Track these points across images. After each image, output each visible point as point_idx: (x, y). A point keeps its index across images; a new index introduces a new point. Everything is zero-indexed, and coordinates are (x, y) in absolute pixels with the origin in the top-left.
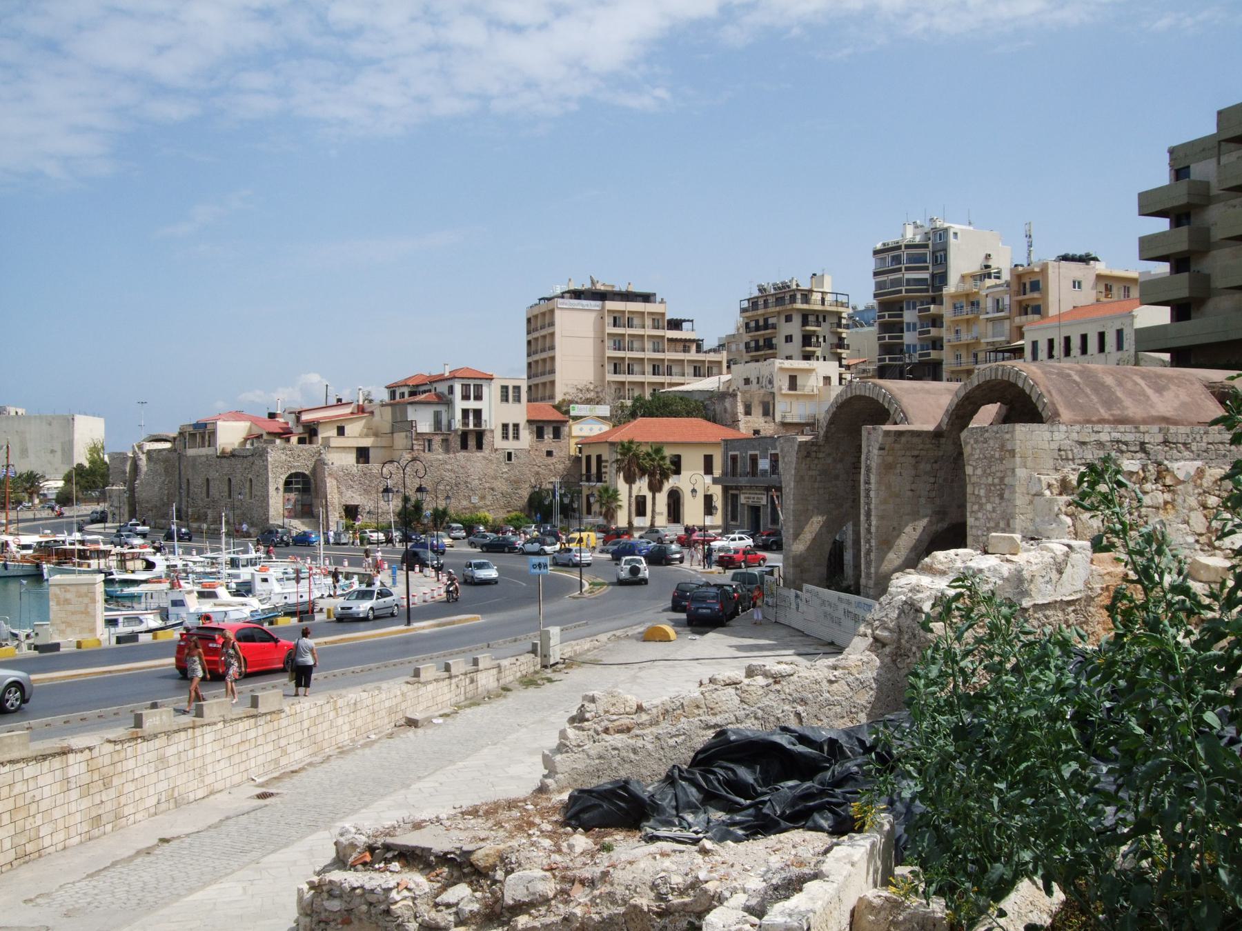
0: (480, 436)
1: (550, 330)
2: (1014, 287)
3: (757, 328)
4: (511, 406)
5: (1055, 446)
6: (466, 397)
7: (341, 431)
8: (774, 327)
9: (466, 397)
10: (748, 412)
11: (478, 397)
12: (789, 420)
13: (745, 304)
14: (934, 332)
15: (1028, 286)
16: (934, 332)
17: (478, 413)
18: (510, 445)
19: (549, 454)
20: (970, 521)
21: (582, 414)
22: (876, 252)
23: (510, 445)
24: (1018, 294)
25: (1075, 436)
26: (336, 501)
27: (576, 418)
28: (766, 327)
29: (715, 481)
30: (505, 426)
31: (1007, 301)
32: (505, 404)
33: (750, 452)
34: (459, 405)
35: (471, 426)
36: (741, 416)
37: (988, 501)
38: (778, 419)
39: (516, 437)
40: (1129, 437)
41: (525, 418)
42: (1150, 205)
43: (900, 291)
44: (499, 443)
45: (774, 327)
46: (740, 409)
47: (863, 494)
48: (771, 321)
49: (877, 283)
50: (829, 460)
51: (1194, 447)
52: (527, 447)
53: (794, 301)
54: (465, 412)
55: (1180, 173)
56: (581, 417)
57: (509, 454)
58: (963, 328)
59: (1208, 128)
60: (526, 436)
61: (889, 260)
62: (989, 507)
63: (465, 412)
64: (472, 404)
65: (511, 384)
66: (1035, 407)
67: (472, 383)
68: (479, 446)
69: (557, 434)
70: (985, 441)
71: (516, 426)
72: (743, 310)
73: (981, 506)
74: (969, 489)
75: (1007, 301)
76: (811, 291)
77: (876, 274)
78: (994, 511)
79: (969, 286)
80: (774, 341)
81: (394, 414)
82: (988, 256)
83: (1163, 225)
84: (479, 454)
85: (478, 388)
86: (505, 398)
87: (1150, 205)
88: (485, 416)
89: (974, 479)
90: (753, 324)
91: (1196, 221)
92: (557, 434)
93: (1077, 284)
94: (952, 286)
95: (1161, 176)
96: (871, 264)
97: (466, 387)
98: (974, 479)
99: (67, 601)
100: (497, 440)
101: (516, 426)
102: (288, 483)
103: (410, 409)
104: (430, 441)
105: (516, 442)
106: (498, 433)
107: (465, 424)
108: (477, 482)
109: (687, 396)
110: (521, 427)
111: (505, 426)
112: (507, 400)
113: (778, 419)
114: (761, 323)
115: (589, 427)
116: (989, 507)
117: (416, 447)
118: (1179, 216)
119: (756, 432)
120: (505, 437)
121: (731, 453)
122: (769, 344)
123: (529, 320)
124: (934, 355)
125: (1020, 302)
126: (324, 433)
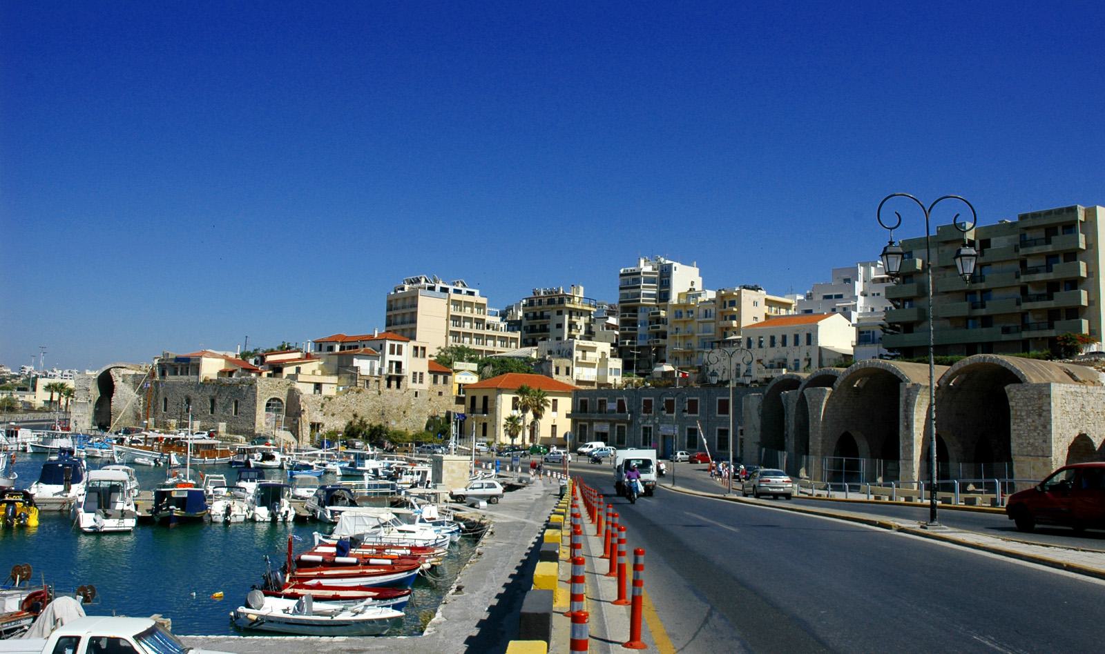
0: (399, 379)
1: (413, 310)
2: (719, 302)
3: (535, 317)
4: (419, 359)
6: (392, 352)
8: (549, 317)
9: (392, 352)
10: (557, 373)
11: (399, 353)
12: (581, 379)
15: (727, 303)
17: (399, 364)
18: (417, 386)
19: (440, 394)
20: (1013, 427)
21: (461, 368)
23: (417, 386)
24: (720, 307)
26: (307, 419)
27: (457, 371)
28: (542, 317)
30: (415, 373)
31: (713, 311)
32: (416, 358)
33: (598, 399)
34: (388, 357)
35: (394, 373)
37: (1028, 416)
38: (575, 378)
39: (421, 382)
41: (427, 370)
43: (639, 301)
44: (411, 385)
45: (549, 317)
46: (554, 370)
48: (545, 314)
49: (621, 294)
50: (836, 401)
52: (427, 389)
54: (391, 362)
56: (1068, 374)
57: (416, 393)
58: (681, 326)
60: (428, 378)
61: (630, 281)
63: (391, 362)
64: (396, 358)
65: (509, 348)
66: (1017, 377)
67: (396, 343)
68: (398, 386)
69: (445, 381)
74: (1012, 412)
75: (713, 311)
79: (683, 301)
80: (548, 327)
81: (339, 361)
82: (692, 283)
84: (398, 391)
85: (400, 347)
90: (531, 315)
93: (755, 304)
94: (674, 299)
96: (618, 282)
97: (392, 347)
99: (453, 471)
100: (408, 382)
102: (268, 405)
104: (368, 381)
105: (421, 385)
107: (390, 370)
108: (395, 410)
109: (505, 359)
110: (424, 375)
111: (415, 373)
112: (417, 356)
113: (575, 378)
114: (538, 314)
115: (465, 377)
116: (1029, 420)
117: (359, 385)
120: (414, 381)
121: (580, 399)
122: (544, 329)
125: (722, 313)
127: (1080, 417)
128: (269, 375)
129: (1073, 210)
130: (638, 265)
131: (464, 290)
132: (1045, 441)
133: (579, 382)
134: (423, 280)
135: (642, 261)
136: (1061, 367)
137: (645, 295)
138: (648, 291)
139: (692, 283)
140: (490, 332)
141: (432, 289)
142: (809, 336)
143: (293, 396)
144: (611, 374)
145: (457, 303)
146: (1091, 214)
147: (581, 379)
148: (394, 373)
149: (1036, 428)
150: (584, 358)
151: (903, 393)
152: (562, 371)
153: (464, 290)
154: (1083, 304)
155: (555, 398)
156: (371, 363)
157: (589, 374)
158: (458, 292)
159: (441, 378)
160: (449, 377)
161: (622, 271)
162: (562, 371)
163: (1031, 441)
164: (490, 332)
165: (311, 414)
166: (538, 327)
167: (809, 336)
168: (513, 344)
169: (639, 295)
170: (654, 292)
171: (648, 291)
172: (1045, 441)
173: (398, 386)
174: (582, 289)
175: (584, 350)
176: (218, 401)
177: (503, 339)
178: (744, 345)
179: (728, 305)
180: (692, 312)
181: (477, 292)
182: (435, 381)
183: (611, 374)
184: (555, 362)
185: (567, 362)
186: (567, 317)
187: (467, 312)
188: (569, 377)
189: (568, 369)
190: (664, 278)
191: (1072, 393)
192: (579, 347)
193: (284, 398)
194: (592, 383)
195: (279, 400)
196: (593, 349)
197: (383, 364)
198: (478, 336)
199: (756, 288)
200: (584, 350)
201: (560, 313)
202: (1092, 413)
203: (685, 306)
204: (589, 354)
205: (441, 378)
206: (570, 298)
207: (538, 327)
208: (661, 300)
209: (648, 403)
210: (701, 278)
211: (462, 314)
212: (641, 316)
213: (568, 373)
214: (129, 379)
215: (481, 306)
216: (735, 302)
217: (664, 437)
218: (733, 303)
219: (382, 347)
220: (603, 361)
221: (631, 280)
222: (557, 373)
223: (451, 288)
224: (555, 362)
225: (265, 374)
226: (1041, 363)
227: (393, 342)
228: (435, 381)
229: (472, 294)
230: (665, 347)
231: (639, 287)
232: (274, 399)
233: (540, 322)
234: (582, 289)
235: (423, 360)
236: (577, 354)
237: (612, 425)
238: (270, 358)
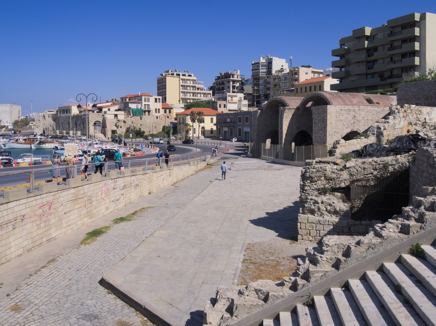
1: (165, 84)
3: (220, 84)
5: (336, 110)
6: (145, 101)
7: (109, 110)
9: (145, 101)
10: (220, 107)
13: (216, 78)
14: (268, 86)
16: (268, 86)
18: (158, 114)
20: (314, 128)
22: (253, 64)
23: (158, 114)
25: (340, 108)
29: (215, 125)
30: (156, 109)
34: (144, 103)
36: (218, 108)
37: (319, 123)
38: (228, 109)
39: (159, 112)
40: (351, 108)
42: (335, 53)
46: (218, 106)
47: (279, 123)
51: (365, 111)
53: (230, 77)
55: (342, 45)
59: (351, 34)
62: (319, 125)
64: (147, 103)
67: (147, 97)
68: (149, 115)
69: (170, 112)
70: (318, 109)
71: (159, 109)
72: (216, 79)
73: (317, 125)
74: (314, 121)
75: (288, 78)
76: (234, 75)
77: (252, 70)
78: (321, 125)
82: (282, 66)
83: (338, 58)
84: (149, 116)
85: (148, 99)
86: (156, 101)
87: (335, 53)
88: (151, 106)
89: (315, 118)
90: (218, 83)
91: (346, 57)
92: (170, 112)
95: (338, 47)
96: (251, 67)
97: (145, 99)
98: (315, 118)
100: (153, 113)
101: (159, 109)
102: (95, 124)
103: (130, 104)
106: (154, 111)
107: (145, 107)
111: (156, 109)
113: (228, 109)
114: (221, 83)
116: (319, 125)
118: (342, 56)
119: (222, 112)
120: (156, 112)
123: (158, 81)
124: (268, 92)
126: (104, 110)
127: (352, 122)
128: (97, 112)
129: (413, 15)
130: (260, 60)
131: (187, 75)
132: (324, 135)
133: (229, 110)
134: (170, 71)
135: (261, 58)
136: (364, 97)
137: (261, 73)
138: (263, 71)
139: (282, 66)
140: (199, 91)
141: (173, 74)
142: (320, 86)
143: (104, 120)
144: (243, 106)
145: (183, 80)
146: (423, 17)
147: (230, 109)
148: (147, 109)
149: (322, 128)
150: (232, 100)
151: (280, 111)
152: (222, 106)
153: (187, 75)
154: (416, 64)
155: (212, 117)
156: (137, 106)
157: (234, 107)
158: (183, 75)
159: (168, 111)
160: (172, 110)
161: (253, 63)
162: (222, 106)
163: (320, 135)
164: (199, 91)
165: (110, 127)
166: (221, 88)
167: (320, 86)
168: (209, 95)
169: (259, 72)
170: (265, 71)
171: (263, 71)
172: (324, 135)
173: (149, 115)
174: (239, 71)
175: (232, 97)
176: (77, 123)
177: (204, 94)
178: (295, 91)
179: (294, 73)
180: (280, 78)
181: (192, 75)
182: (165, 112)
183: (243, 106)
184: (219, 103)
185: (224, 102)
186: (231, 83)
187: (188, 83)
188: (225, 108)
189: (225, 105)
190: (269, 64)
191: (345, 110)
192: (229, 96)
193: (101, 121)
194: (236, 110)
195: (99, 122)
196: (236, 96)
197: (142, 106)
198: (194, 93)
199: (309, 67)
200: (232, 97)
201: (229, 82)
202: (363, 120)
203: (277, 76)
204: (234, 98)
205: (168, 111)
206: (233, 75)
207: (221, 88)
208: (268, 74)
209: (240, 118)
210: (287, 64)
211: (186, 84)
212: (261, 82)
213: (225, 107)
214: (50, 116)
215: (194, 81)
216: (297, 73)
217: (246, 132)
218: (296, 74)
219: (141, 99)
220: (240, 101)
221: (256, 66)
222: (220, 107)
223: (181, 74)
224: (219, 103)
225: (96, 112)
226: (350, 95)
227: (145, 97)
228: (165, 112)
229: (190, 76)
230: (269, 94)
231: (259, 69)
232: (97, 121)
233: (220, 87)
234: (239, 71)
235: (159, 103)
236: (229, 98)
237: (229, 128)
238: (98, 105)
